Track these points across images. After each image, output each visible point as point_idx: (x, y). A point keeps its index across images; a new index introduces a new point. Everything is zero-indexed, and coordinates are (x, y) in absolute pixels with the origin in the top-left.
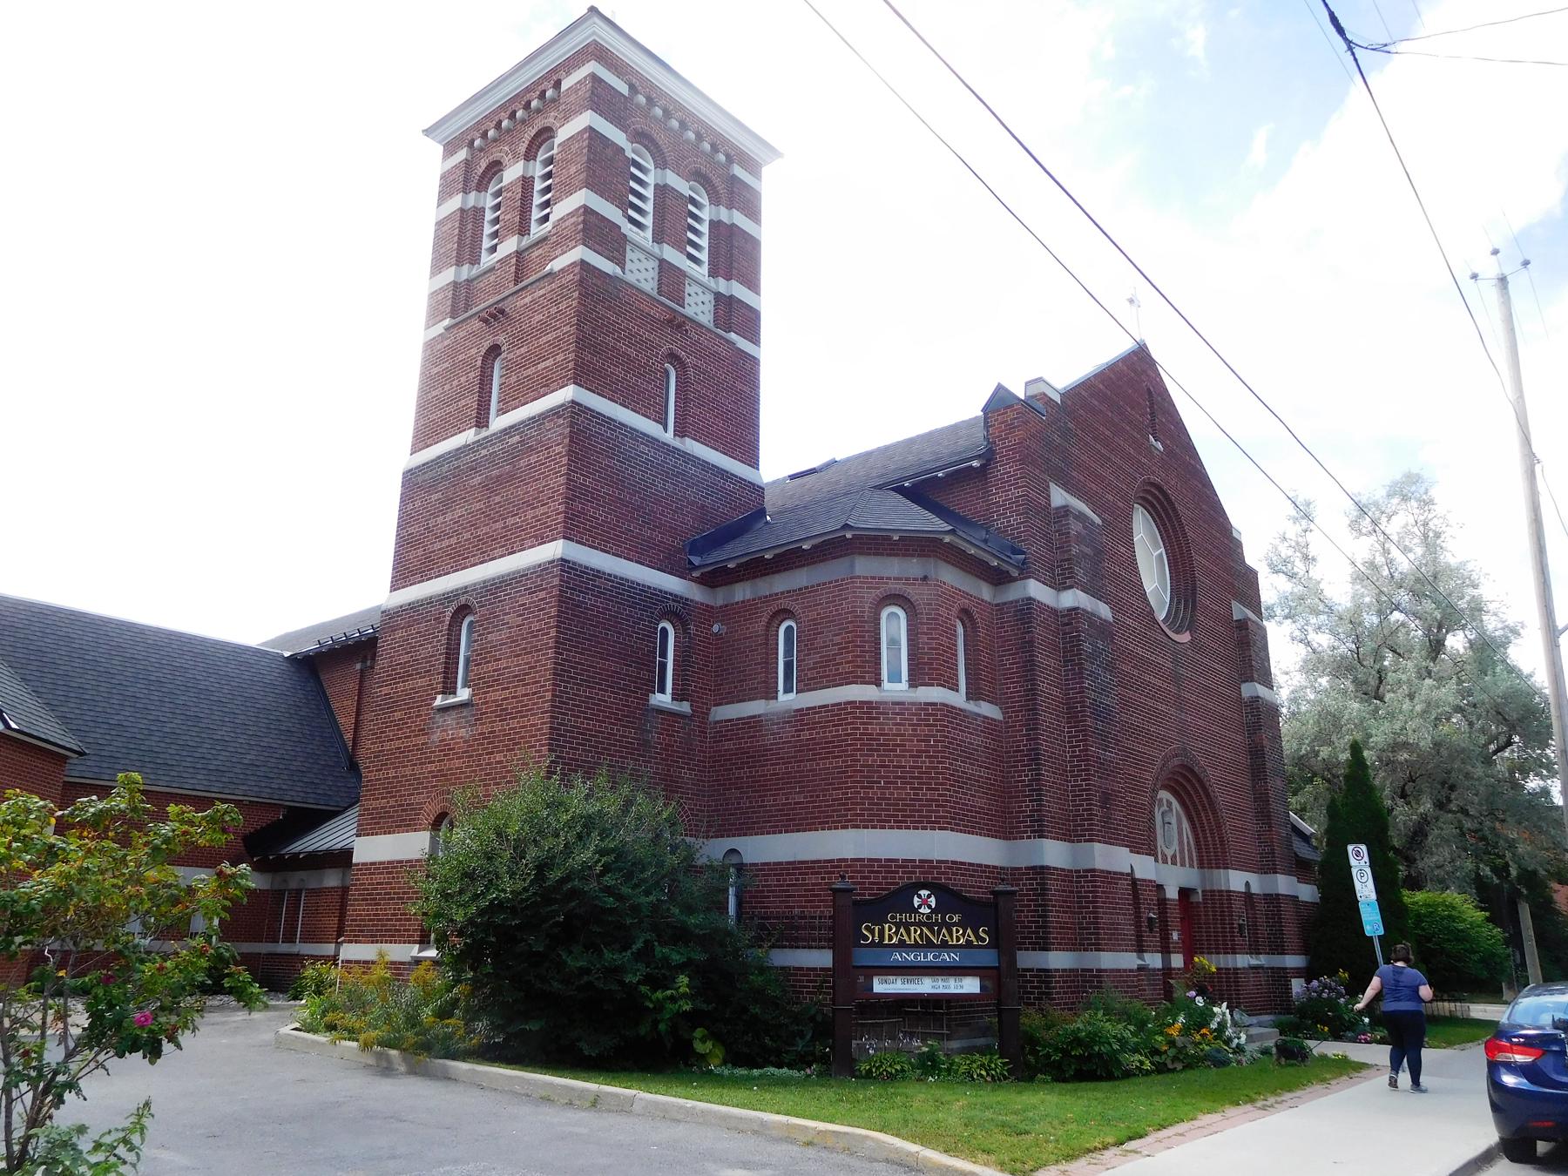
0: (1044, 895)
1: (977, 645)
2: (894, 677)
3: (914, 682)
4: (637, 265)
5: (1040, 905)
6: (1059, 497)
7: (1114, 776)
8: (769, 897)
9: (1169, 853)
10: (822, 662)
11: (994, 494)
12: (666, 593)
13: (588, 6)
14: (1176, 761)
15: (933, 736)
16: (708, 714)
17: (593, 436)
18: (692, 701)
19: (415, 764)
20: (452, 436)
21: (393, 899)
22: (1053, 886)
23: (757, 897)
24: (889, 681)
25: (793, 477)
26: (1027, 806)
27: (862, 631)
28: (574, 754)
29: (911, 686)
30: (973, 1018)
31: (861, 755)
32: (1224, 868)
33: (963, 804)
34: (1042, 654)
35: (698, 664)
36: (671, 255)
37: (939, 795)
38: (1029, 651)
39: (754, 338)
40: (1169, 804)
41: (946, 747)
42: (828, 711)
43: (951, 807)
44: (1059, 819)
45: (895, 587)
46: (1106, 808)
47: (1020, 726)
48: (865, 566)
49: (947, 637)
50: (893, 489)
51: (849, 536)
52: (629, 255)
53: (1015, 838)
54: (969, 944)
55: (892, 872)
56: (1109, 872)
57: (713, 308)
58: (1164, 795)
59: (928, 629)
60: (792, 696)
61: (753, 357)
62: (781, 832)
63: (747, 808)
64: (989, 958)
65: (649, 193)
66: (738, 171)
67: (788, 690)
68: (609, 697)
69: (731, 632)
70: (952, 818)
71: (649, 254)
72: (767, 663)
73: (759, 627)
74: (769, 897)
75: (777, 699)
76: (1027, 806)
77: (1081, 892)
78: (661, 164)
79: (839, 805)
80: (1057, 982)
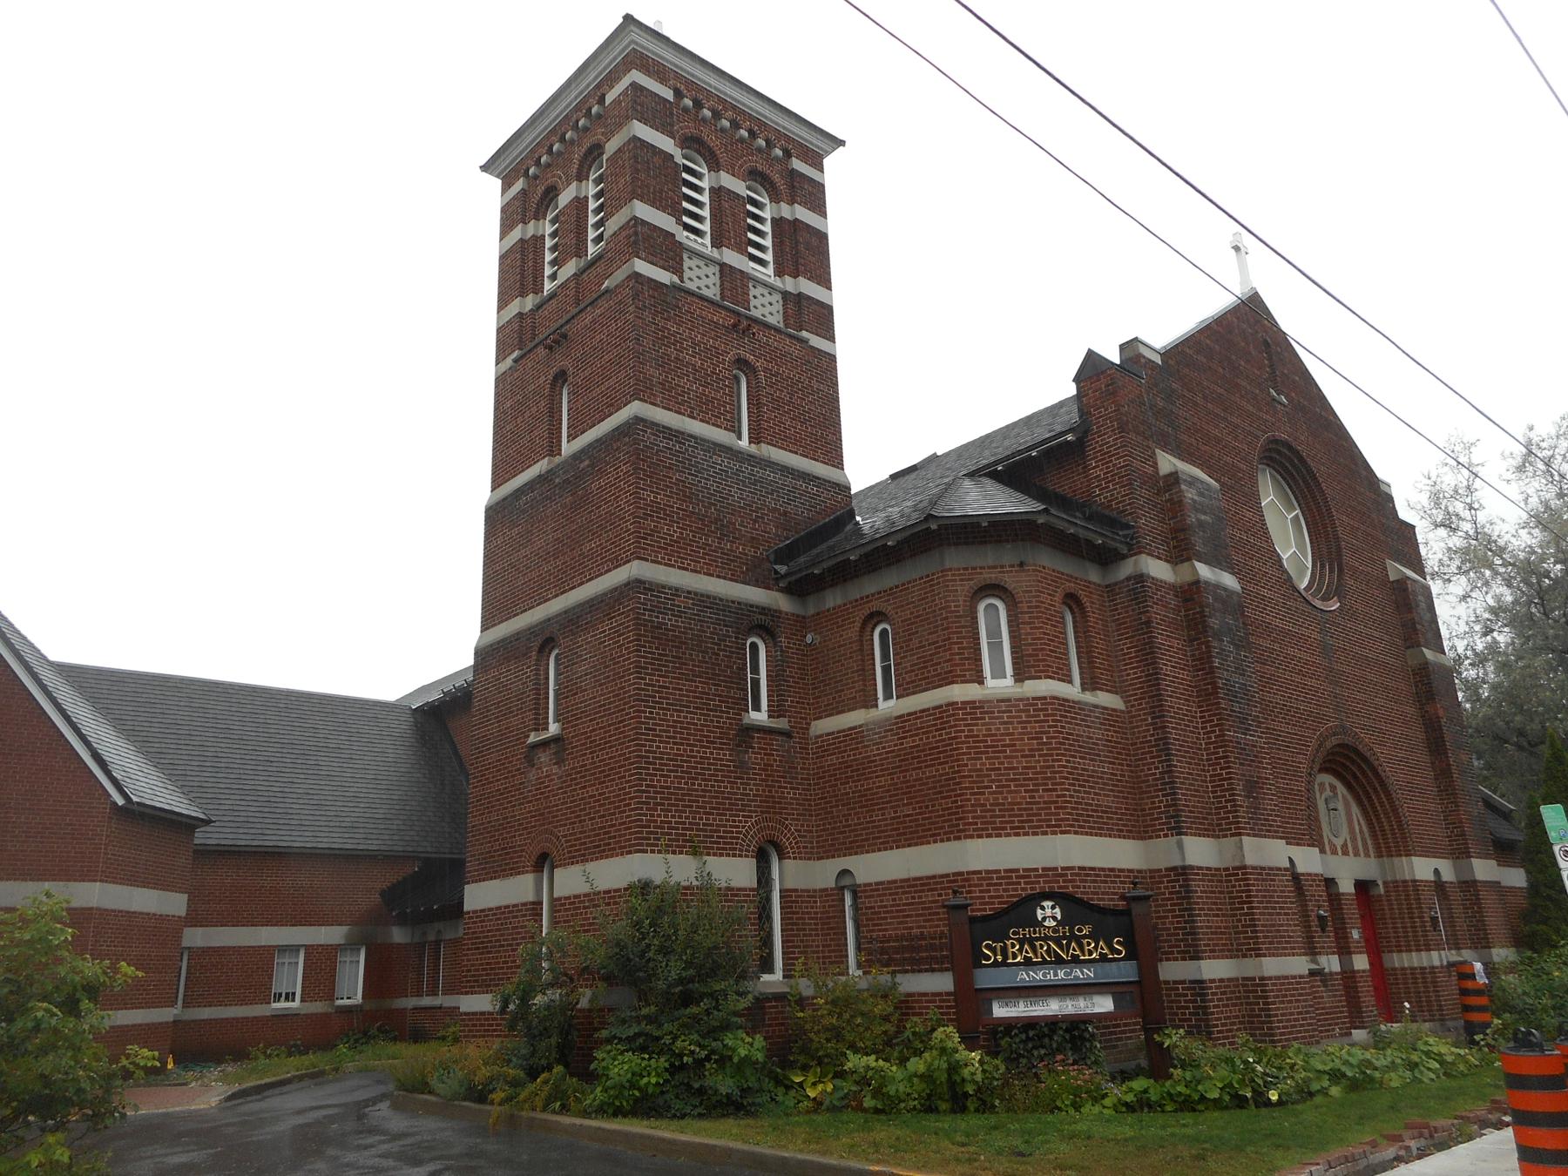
0: (1189, 898)
1: (1089, 631)
2: (999, 673)
3: (1020, 677)
4: (761, 300)
5: (1186, 910)
6: (1167, 463)
7: (1259, 762)
8: (886, 918)
9: (1339, 842)
10: (920, 663)
11: (1094, 468)
12: (752, 606)
13: (624, 14)
14: (1334, 741)
15: (1045, 733)
16: (808, 729)
17: (661, 451)
18: (789, 717)
19: (514, 806)
20: (528, 467)
21: (503, 946)
22: (1198, 886)
23: (874, 919)
24: (992, 678)
25: (894, 477)
26: (1161, 801)
27: (958, 627)
28: (666, 782)
29: (1016, 681)
30: (1120, 1039)
31: (968, 759)
32: (1407, 855)
33: (1086, 804)
34: (1162, 634)
35: (794, 677)
36: (732, 258)
37: (1058, 796)
38: (1146, 633)
39: (830, 335)
40: (1333, 788)
41: (1060, 743)
42: (930, 715)
43: (1073, 808)
44: (1199, 813)
45: (990, 576)
46: (1254, 797)
47: (1144, 714)
48: (955, 559)
49: (1052, 625)
50: (985, 475)
51: (934, 527)
52: (687, 263)
53: (1151, 837)
54: (1103, 958)
55: (1013, 884)
56: (1263, 868)
57: (781, 308)
58: (1327, 779)
59: (1030, 618)
60: (892, 702)
61: (829, 354)
62: (892, 848)
63: (855, 825)
64: (1126, 971)
65: (705, 198)
66: (797, 164)
67: (888, 696)
68: (699, 720)
69: (825, 641)
70: (1074, 820)
71: (709, 260)
72: (863, 670)
73: (852, 633)
74: (886, 918)
75: (877, 706)
76: (1161, 801)
77: (1232, 892)
78: (714, 166)
79: (949, 814)
80: (1213, 994)
